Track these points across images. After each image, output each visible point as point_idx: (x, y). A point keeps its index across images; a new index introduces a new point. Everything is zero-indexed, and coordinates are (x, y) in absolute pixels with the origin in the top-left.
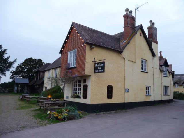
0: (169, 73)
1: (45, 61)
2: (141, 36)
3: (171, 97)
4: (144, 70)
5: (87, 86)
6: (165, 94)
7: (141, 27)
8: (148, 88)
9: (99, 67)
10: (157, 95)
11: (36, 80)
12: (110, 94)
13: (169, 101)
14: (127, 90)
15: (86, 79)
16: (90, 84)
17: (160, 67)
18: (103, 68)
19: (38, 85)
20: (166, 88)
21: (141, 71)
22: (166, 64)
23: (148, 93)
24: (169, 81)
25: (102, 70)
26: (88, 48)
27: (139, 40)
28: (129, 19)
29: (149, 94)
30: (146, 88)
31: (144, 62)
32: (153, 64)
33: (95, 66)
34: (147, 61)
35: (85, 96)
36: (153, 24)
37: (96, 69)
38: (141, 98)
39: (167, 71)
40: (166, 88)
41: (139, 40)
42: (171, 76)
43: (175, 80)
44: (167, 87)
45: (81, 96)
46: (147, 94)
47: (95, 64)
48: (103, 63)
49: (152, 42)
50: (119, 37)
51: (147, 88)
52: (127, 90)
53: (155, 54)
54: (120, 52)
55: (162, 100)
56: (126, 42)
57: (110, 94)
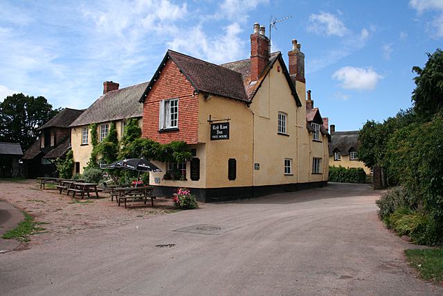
0: (323, 134)
1: (58, 102)
2: (279, 71)
3: (324, 177)
4: (282, 132)
5: (199, 160)
6: (315, 172)
7: (279, 57)
8: (289, 161)
9: (220, 130)
10: (302, 174)
11: (43, 146)
12: (232, 175)
13: (321, 185)
14: (257, 166)
15: (195, 150)
16: (204, 157)
17: (309, 125)
18: (226, 132)
19: (52, 159)
20: (316, 161)
21: (278, 134)
22: (318, 119)
23: (287, 170)
24: (321, 149)
25: (226, 136)
26: (200, 98)
27: (276, 79)
28: (261, 44)
29: (289, 172)
30: (286, 161)
31: (282, 117)
32: (298, 120)
33: (212, 128)
34: (287, 114)
35: (195, 176)
36: (299, 46)
37: (213, 132)
38: (279, 179)
39: (320, 133)
40: (316, 161)
41: (276, 79)
42: (325, 142)
43: (334, 144)
44: (319, 159)
45: (188, 176)
46: (286, 172)
47: (212, 125)
48: (227, 124)
49: (297, 81)
50: (239, 71)
51: (287, 163)
52: (257, 166)
53: (300, 102)
54: (248, 104)
55: (422, 66)
56: (255, 85)
57: (232, 175)
